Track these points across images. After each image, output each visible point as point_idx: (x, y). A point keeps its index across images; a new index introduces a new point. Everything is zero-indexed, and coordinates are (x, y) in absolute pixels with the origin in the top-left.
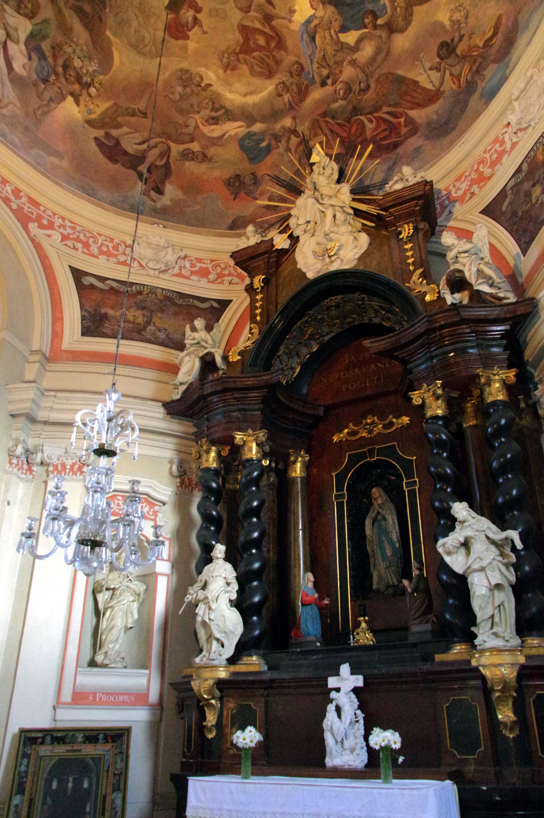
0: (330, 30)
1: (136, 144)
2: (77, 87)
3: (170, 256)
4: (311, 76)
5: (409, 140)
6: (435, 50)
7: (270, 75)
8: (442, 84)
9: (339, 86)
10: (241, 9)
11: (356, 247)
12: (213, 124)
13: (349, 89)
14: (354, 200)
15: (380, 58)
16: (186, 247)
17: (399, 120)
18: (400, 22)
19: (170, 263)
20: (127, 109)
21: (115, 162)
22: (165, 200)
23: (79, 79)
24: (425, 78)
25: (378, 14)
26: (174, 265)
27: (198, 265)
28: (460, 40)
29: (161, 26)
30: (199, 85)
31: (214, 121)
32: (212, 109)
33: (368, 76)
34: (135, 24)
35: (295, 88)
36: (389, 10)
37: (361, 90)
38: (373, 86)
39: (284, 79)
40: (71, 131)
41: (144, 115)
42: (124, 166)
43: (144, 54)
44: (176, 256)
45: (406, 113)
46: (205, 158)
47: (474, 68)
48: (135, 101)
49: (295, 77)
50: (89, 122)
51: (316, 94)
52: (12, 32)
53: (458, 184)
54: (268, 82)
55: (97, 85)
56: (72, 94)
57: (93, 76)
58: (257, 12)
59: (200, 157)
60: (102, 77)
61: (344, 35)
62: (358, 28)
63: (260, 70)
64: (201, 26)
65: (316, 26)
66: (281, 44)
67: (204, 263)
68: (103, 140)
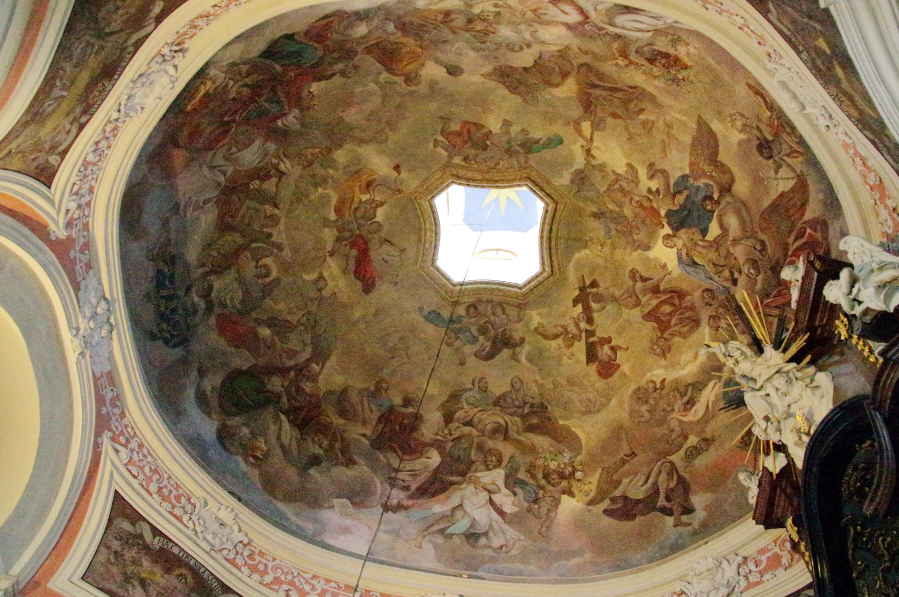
0: (696, 244)
1: (643, 485)
2: (564, 483)
3: (730, 571)
4: (721, 288)
5: (830, 237)
6: (761, 159)
7: (696, 323)
8: (793, 170)
9: (745, 269)
10: (635, 306)
11: (823, 397)
12: (692, 407)
13: (754, 263)
14: (784, 351)
15: (745, 214)
16: (738, 549)
17: (807, 234)
18: (725, 178)
19: (731, 579)
20: (615, 463)
21: (634, 516)
22: (700, 514)
23: (562, 476)
24: (783, 183)
25: (708, 194)
26: (737, 578)
27: (764, 558)
28: (761, 132)
29: (594, 377)
30: (656, 389)
31: (690, 403)
32: (682, 396)
33: (753, 236)
34: (575, 398)
35: (721, 310)
36: (710, 182)
37: (760, 251)
38: (763, 237)
39: (708, 313)
40: (579, 524)
41: (633, 454)
42: (643, 515)
43: (599, 411)
44: (734, 567)
45: (804, 223)
46: (707, 442)
47: (788, 130)
48: (620, 449)
49: (713, 303)
50: (591, 503)
51: (741, 294)
52: (491, 487)
53: (881, 219)
54: (700, 329)
55: (579, 467)
56: (564, 492)
57: (571, 464)
58: (645, 295)
59: (703, 445)
60: (578, 458)
61: (708, 235)
62: (710, 220)
63: (686, 329)
64: (621, 348)
65: (687, 255)
66: (680, 294)
67: (769, 550)
68: (612, 507)
